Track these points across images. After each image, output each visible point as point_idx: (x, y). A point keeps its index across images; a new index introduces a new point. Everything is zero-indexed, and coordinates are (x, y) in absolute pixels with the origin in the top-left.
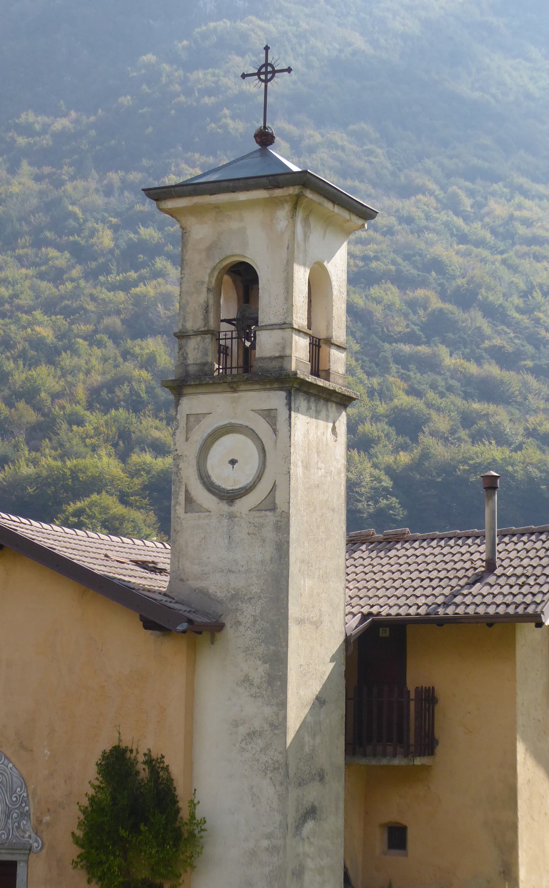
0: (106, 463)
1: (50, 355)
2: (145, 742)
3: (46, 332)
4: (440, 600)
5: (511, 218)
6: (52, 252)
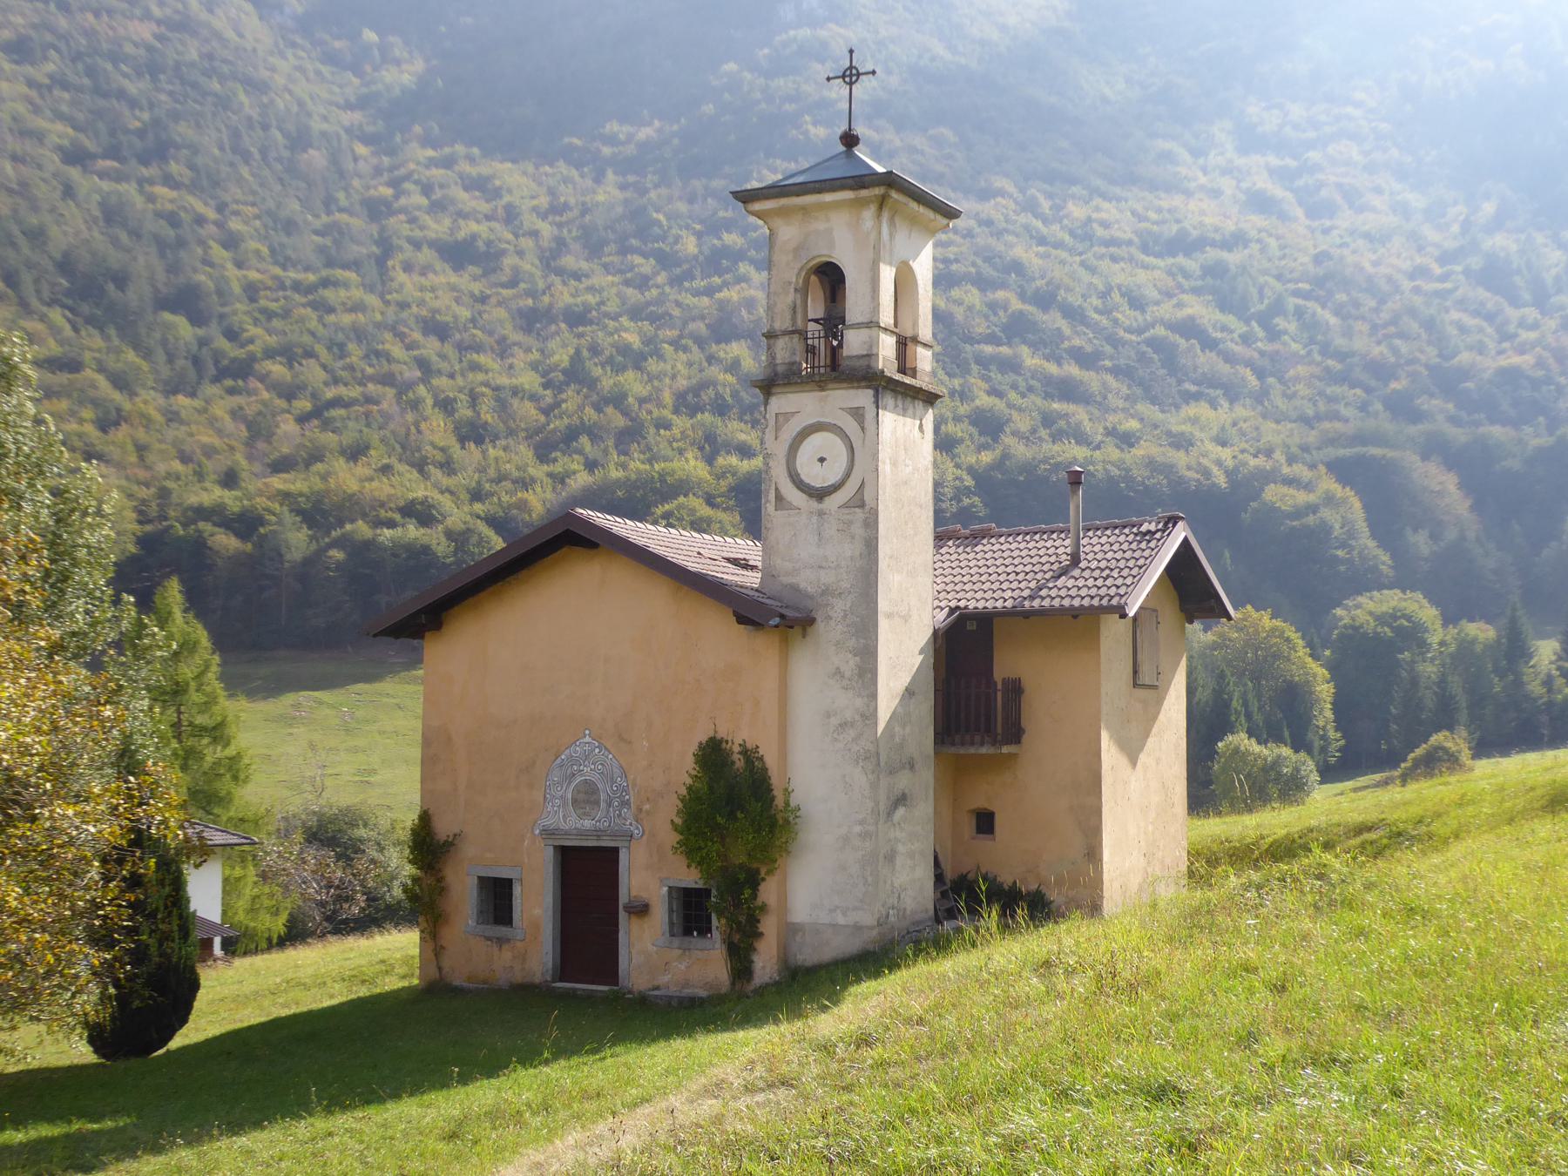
0: (692, 466)
1: (635, 359)
2: (740, 733)
3: (633, 339)
4: (1026, 593)
5: (1089, 220)
6: (638, 260)
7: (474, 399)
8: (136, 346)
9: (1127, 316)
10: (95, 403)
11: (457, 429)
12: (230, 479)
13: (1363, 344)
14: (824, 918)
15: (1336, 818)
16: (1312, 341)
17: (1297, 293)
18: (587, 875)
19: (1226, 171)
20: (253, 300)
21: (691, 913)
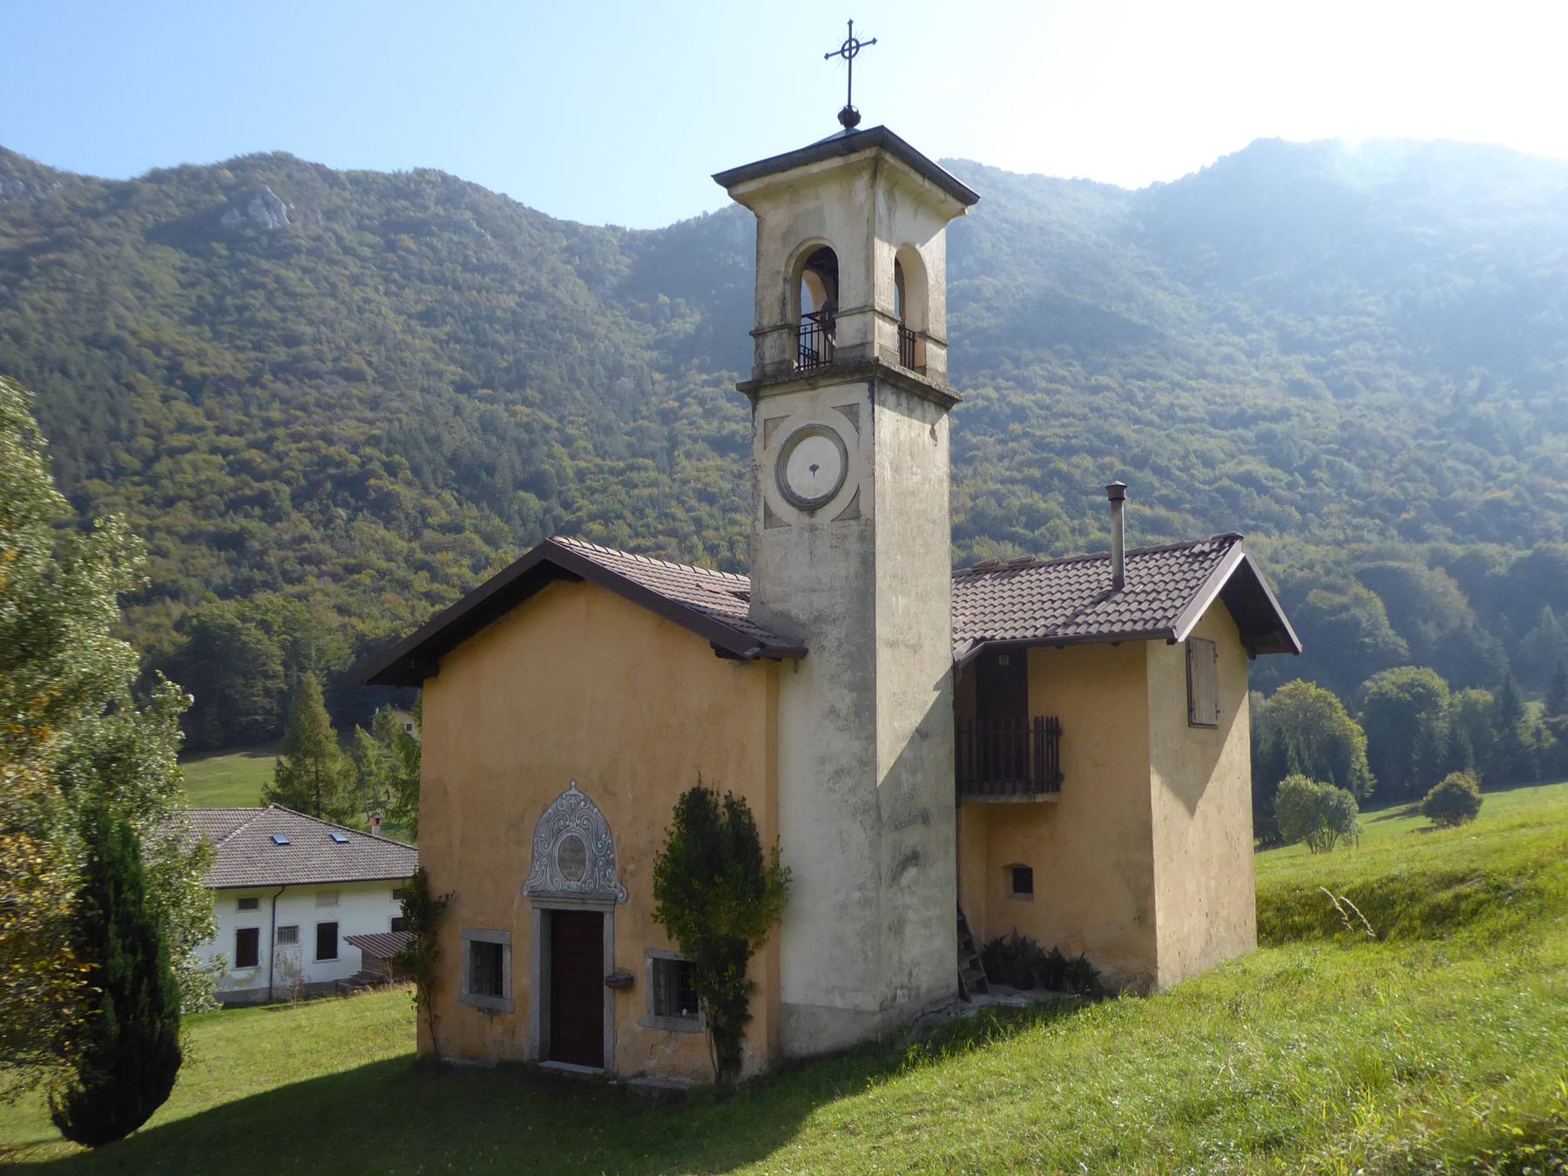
2: (732, 781)
4: (1060, 621)
5: (1172, 404)
7: (732, 545)
9: (1201, 472)
10: (472, 554)
13: (1381, 486)
14: (822, 1000)
15: (1418, 867)
16: (1341, 485)
17: (1328, 452)
18: (573, 937)
19: (1274, 367)
20: (582, 481)
21: (680, 988)
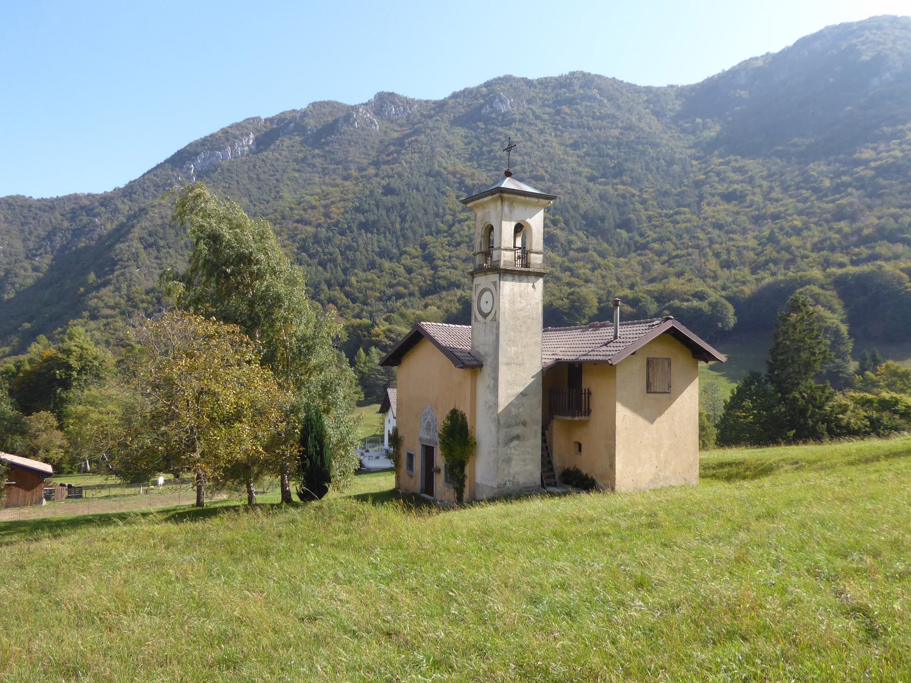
0: (816, 273)
1: (797, 231)
2: (465, 409)
3: (798, 224)
6: (804, 191)
7: (729, 251)
8: (607, 242)
10: (592, 262)
11: (721, 264)
12: (632, 287)
